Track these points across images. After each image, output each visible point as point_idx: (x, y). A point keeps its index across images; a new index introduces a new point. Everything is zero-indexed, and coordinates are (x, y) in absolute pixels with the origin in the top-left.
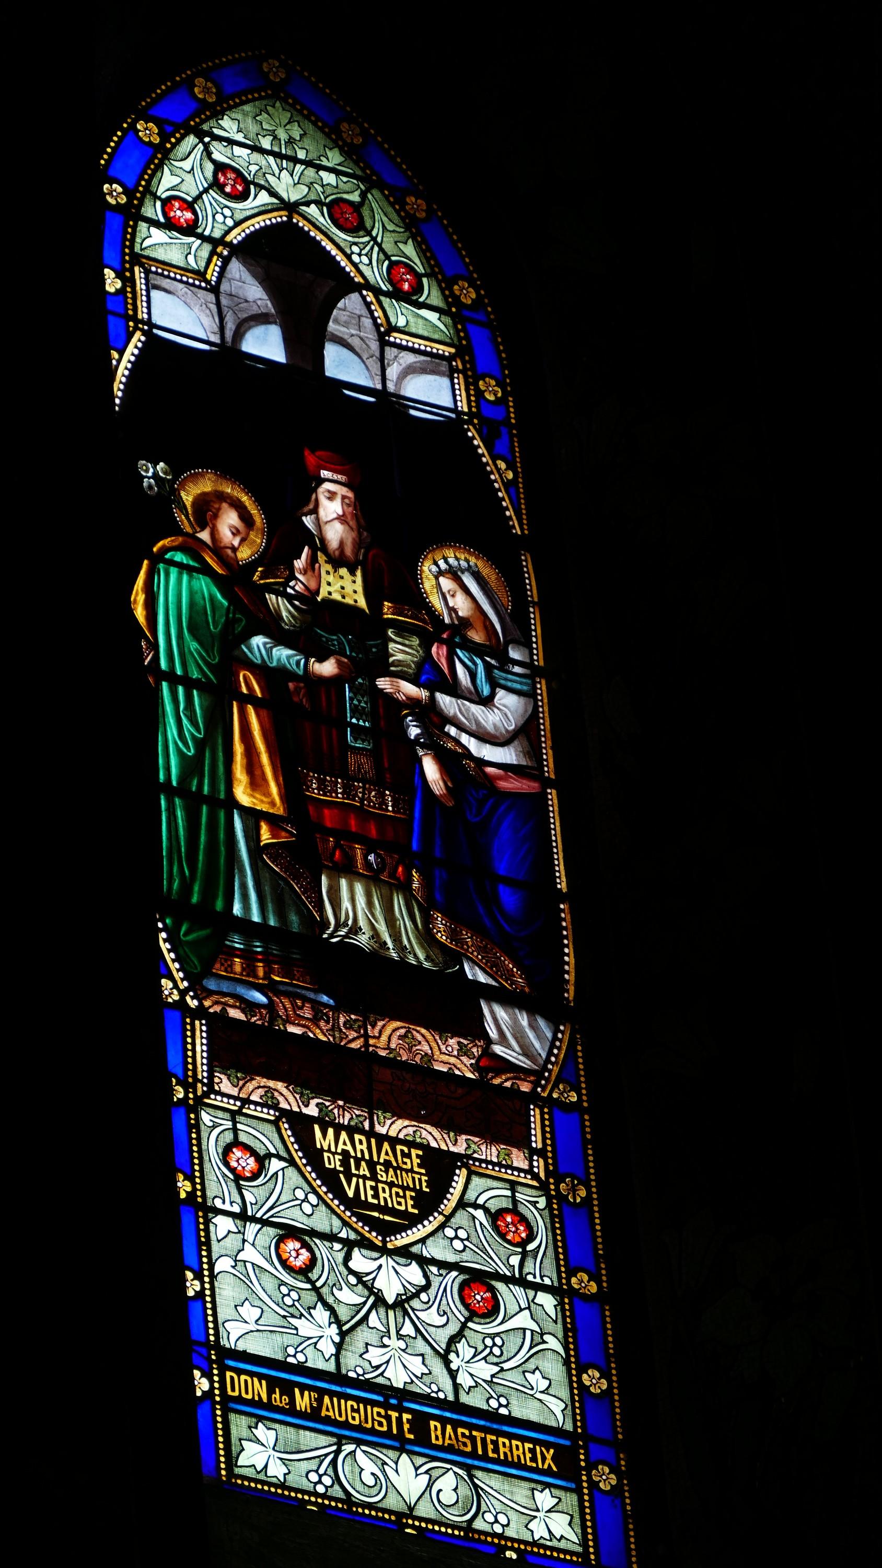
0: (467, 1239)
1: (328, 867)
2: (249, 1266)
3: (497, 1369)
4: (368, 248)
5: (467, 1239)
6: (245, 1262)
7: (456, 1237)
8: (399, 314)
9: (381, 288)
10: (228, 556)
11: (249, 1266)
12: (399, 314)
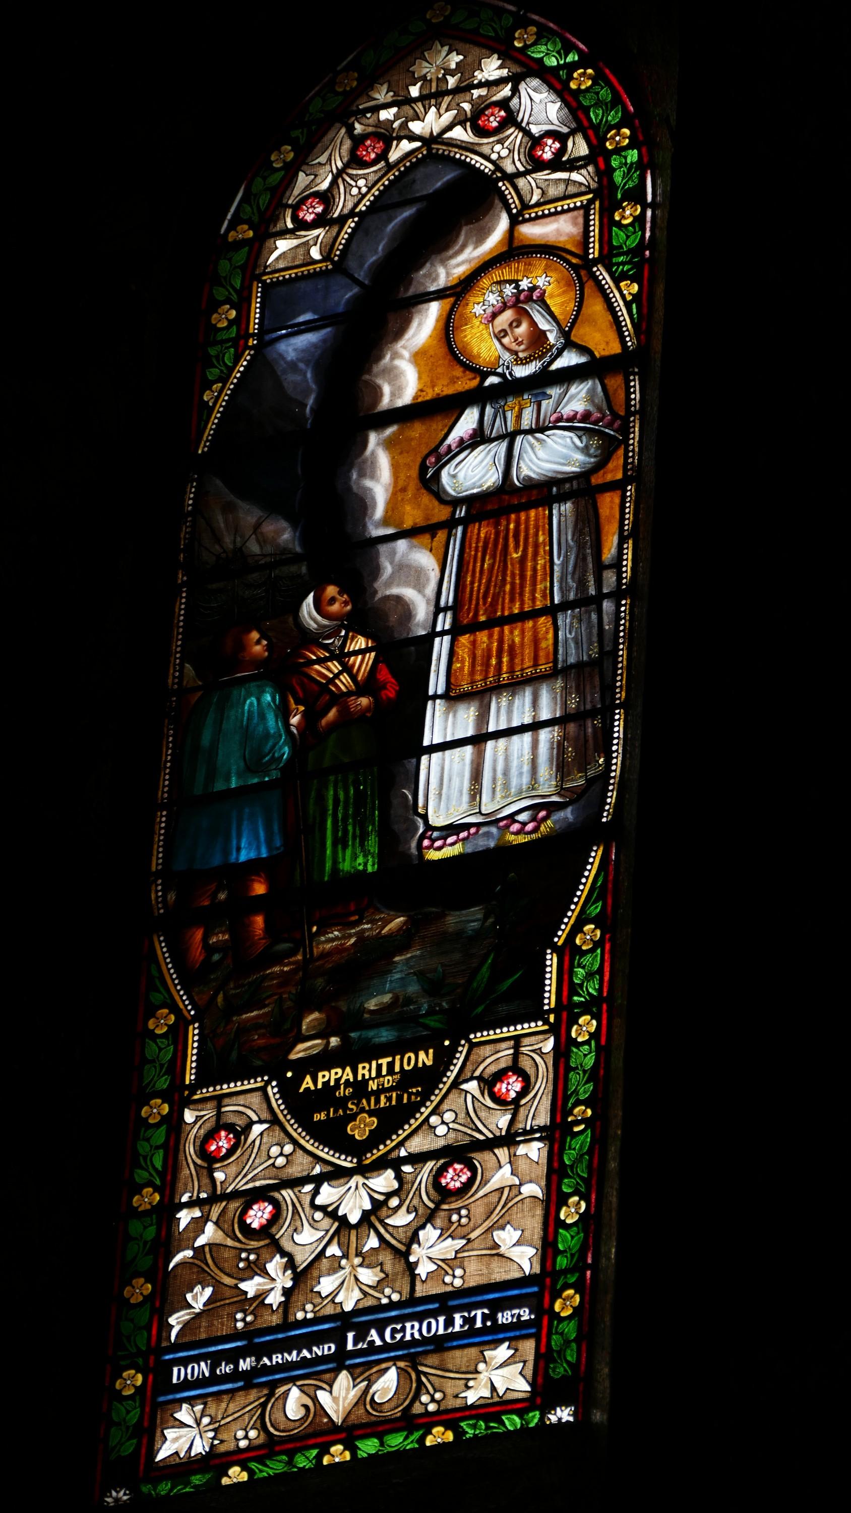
0: (459, 1225)
1: (226, 852)
2: (469, 1097)
3: (464, 1242)
4: (348, 179)
5: (459, 1225)
6: (467, 1092)
7: (461, 1217)
8: (520, 1198)
9: (319, 664)
10: (312, 373)
11: (469, 1097)
12: (520, 1198)
